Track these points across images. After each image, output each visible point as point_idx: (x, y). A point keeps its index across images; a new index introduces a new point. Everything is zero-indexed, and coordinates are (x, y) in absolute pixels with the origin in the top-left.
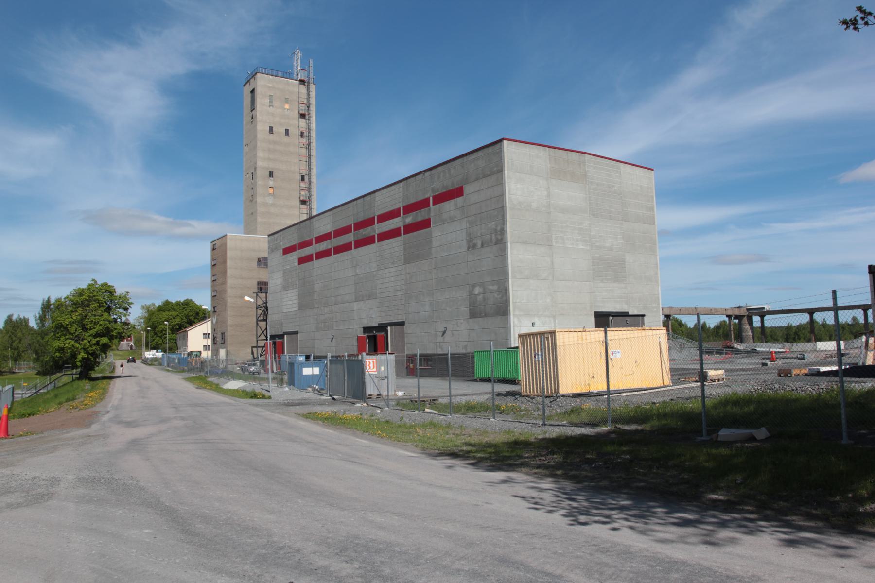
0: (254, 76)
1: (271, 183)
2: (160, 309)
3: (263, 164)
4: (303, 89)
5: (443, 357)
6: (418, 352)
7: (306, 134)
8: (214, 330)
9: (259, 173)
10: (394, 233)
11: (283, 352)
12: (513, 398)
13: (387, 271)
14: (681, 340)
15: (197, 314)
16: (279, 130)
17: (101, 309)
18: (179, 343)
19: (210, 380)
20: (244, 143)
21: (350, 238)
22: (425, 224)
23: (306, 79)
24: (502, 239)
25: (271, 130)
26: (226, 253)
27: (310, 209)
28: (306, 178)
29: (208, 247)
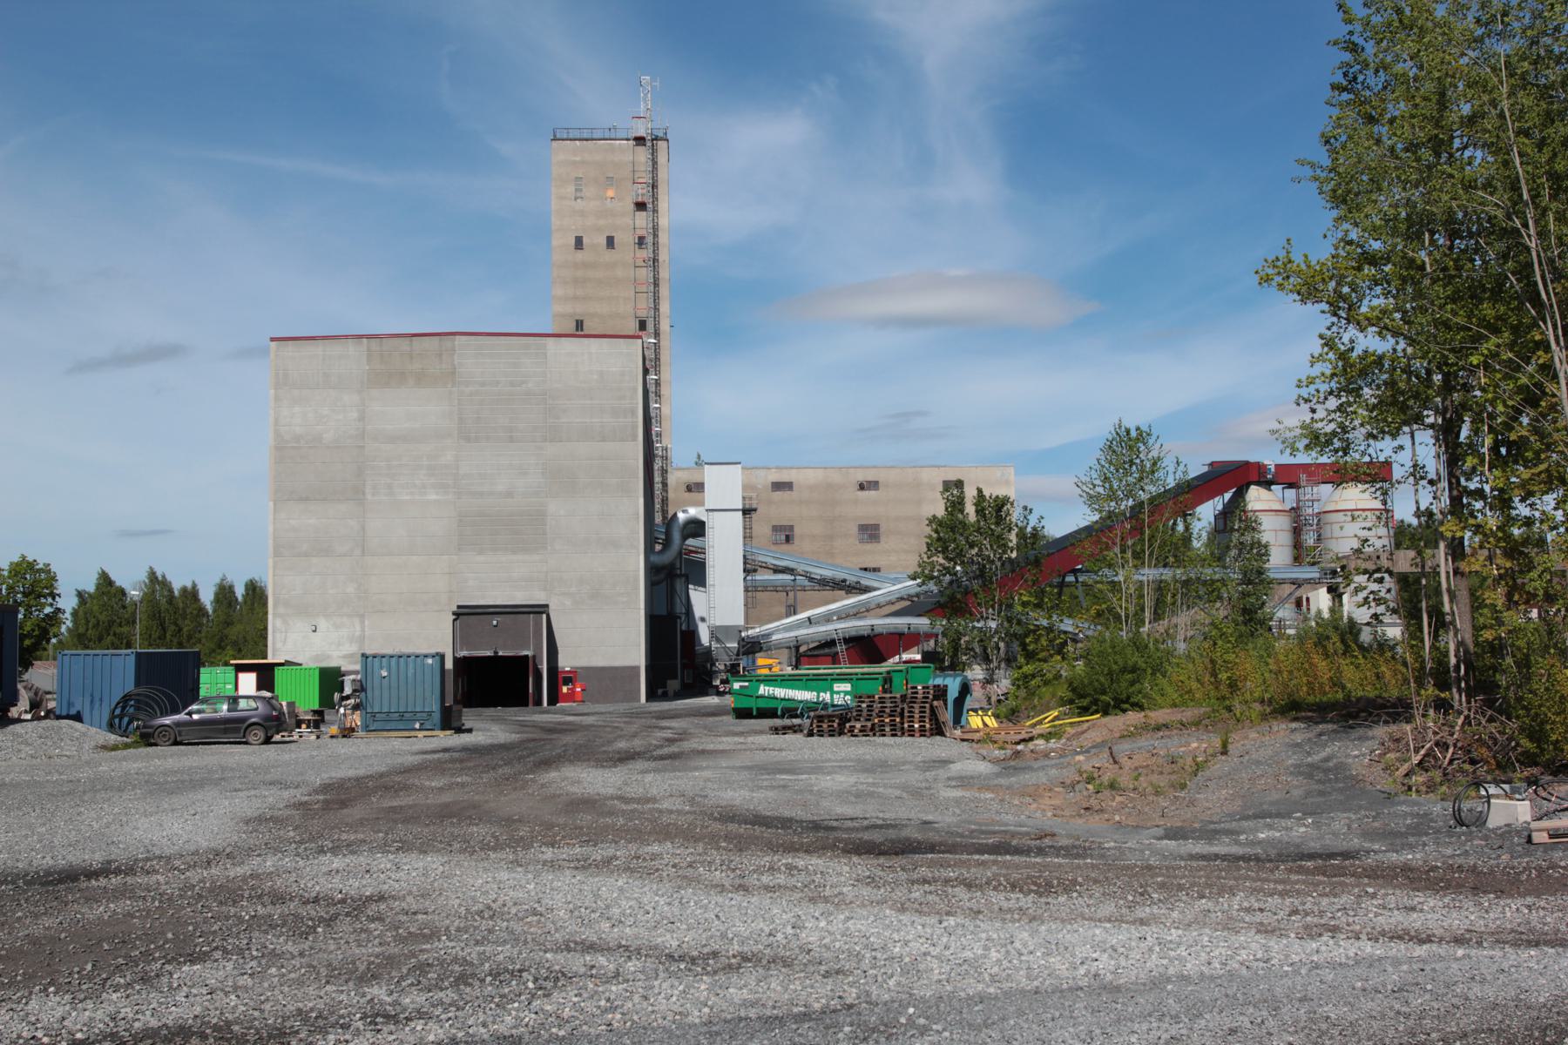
7: (650, 240)
25: (579, 243)
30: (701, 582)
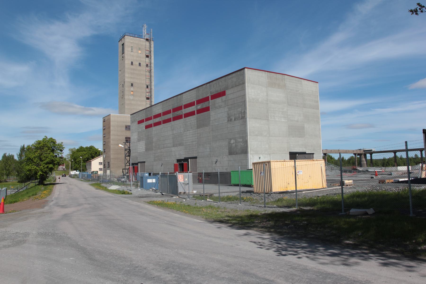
0: (123, 37)
1: (132, 89)
2: (78, 151)
3: (128, 80)
4: (147, 43)
5: (216, 174)
6: (204, 172)
7: (149, 65)
8: (104, 161)
9: (126, 84)
10: (192, 114)
11: (138, 172)
12: (250, 194)
13: (188, 132)
14: (332, 166)
15: (96, 153)
16: (136, 63)
17: (49, 150)
18: (87, 167)
19: (102, 185)
20: (119, 70)
21: (170, 116)
22: (207, 109)
23: (149, 39)
24: (244, 116)
25: (132, 63)
26: (110, 123)
27: (151, 102)
28: (149, 87)
29: (101, 120)
30: (29, 146)
